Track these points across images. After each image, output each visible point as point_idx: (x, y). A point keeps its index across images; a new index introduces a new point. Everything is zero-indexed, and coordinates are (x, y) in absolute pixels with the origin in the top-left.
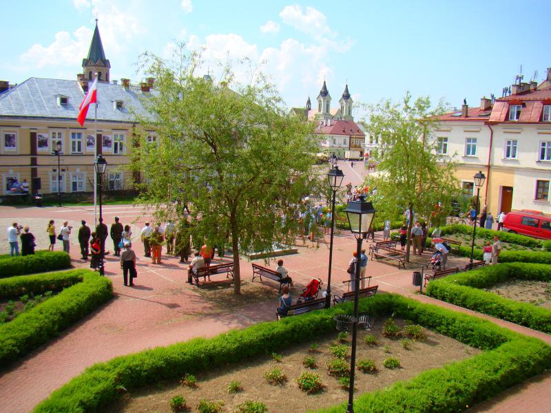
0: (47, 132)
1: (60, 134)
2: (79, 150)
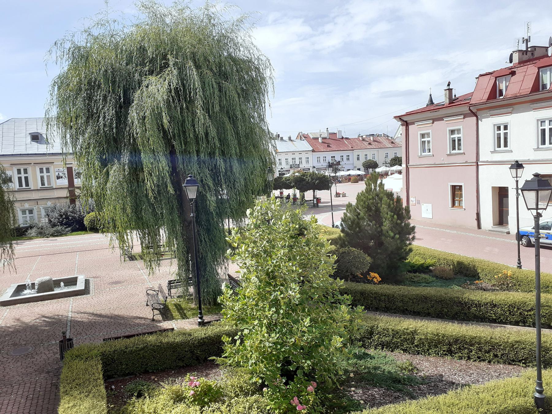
0: (12, 170)
1: (26, 171)
2: (27, 184)
